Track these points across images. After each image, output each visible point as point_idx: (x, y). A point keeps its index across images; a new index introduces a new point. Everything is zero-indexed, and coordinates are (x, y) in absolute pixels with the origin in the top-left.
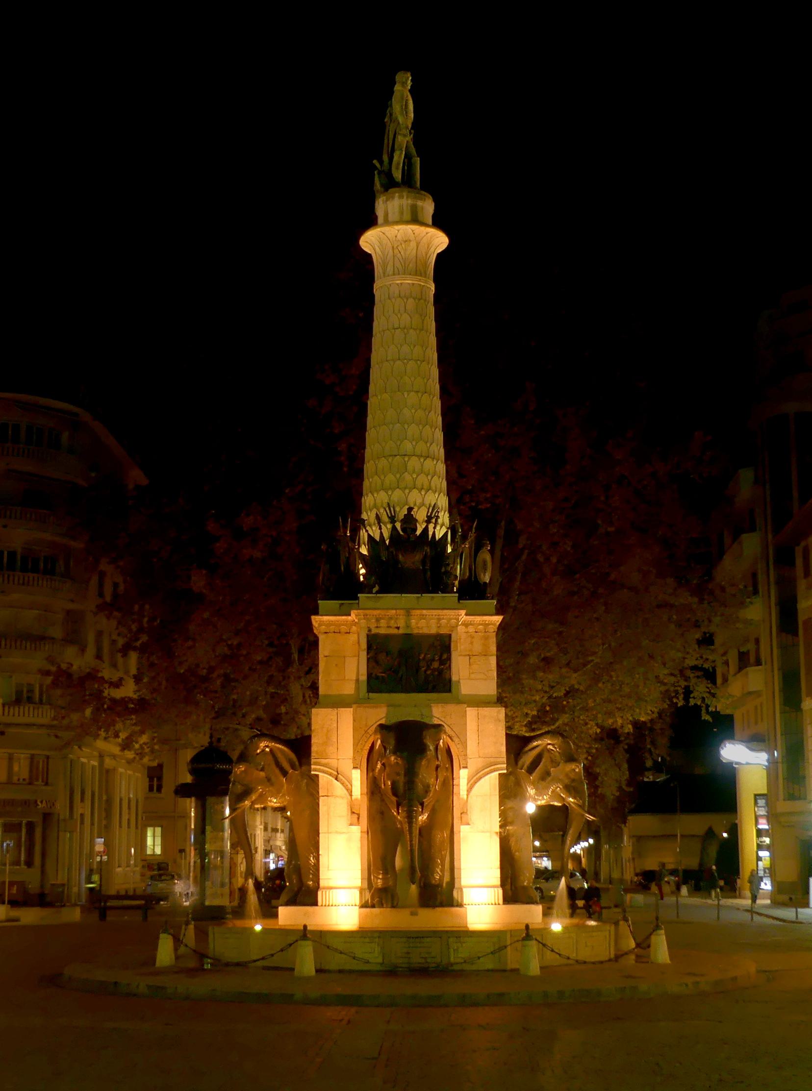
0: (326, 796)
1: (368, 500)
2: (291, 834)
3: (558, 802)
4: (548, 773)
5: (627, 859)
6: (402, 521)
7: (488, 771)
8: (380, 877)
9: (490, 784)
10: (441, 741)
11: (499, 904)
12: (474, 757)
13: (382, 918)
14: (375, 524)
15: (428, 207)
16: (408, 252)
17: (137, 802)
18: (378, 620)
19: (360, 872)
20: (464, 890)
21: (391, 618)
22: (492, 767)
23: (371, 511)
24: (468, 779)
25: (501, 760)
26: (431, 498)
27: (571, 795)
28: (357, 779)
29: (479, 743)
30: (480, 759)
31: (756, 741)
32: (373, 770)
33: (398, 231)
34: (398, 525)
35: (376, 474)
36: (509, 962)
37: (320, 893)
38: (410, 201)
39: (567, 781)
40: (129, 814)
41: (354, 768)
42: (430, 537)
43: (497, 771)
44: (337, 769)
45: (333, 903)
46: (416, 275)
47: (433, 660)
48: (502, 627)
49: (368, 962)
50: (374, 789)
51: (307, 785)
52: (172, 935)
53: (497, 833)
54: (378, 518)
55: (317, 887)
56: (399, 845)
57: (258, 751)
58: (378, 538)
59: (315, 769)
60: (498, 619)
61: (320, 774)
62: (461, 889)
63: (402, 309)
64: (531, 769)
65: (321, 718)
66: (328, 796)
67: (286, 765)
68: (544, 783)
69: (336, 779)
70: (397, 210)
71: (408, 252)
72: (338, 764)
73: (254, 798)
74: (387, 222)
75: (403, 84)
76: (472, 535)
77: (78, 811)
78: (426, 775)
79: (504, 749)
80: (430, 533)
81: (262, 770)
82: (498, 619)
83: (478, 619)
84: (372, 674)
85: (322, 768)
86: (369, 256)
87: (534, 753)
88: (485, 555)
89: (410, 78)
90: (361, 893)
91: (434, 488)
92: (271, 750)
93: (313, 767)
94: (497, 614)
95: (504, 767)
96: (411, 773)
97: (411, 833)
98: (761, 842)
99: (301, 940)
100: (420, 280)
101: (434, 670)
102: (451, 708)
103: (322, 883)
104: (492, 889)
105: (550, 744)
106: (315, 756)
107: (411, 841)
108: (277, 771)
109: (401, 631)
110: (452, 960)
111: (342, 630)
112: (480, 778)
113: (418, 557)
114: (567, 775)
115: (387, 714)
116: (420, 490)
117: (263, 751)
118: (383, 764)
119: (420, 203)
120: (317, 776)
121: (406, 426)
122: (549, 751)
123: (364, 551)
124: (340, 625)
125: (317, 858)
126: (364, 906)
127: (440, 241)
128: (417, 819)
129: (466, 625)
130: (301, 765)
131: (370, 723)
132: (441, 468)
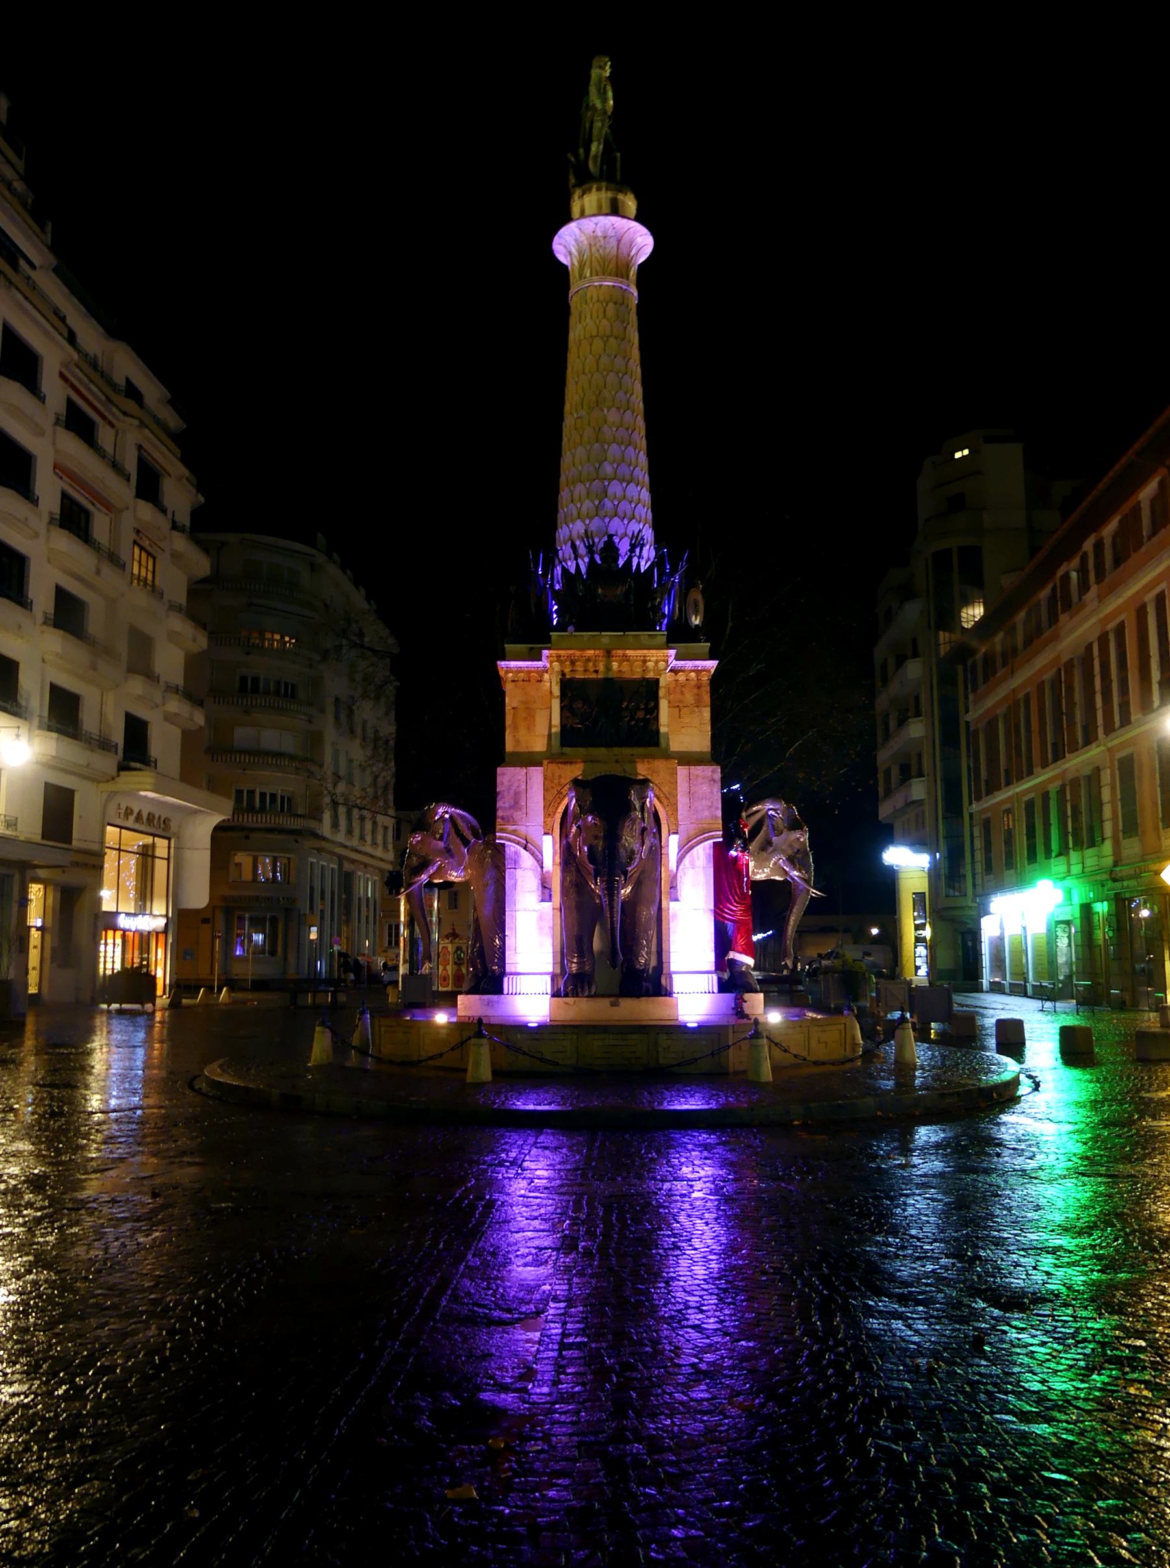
1: (562, 533)
4: (768, 843)
8: (575, 960)
9: (702, 854)
10: (648, 800)
13: (580, 1009)
14: (570, 559)
15: (630, 203)
16: (608, 251)
17: (375, 901)
18: (573, 663)
19: (551, 956)
20: (674, 976)
21: (588, 660)
23: (566, 544)
25: (716, 826)
26: (634, 527)
27: (795, 868)
28: (549, 846)
31: (919, 843)
32: (567, 836)
33: (596, 224)
35: (572, 502)
36: (731, 1065)
37: (506, 979)
38: (610, 194)
39: (790, 852)
40: (368, 911)
41: (546, 834)
42: (634, 568)
43: (708, 839)
46: (617, 276)
47: (638, 708)
48: (716, 680)
49: (557, 1064)
50: (567, 857)
51: (492, 857)
52: (329, 1028)
55: (503, 973)
56: (666, 1106)
58: (573, 571)
59: (501, 837)
60: (712, 664)
61: (507, 843)
62: (670, 976)
63: (601, 315)
65: (507, 777)
67: (467, 834)
68: (765, 854)
69: (525, 848)
70: (595, 204)
71: (608, 251)
73: (431, 872)
74: (583, 215)
75: (602, 70)
76: (682, 567)
77: (318, 906)
78: (629, 839)
79: (719, 813)
81: (441, 839)
82: (712, 664)
83: (689, 664)
84: (566, 725)
87: (753, 820)
88: (696, 595)
89: (609, 63)
90: (552, 980)
91: (638, 517)
92: (451, 817)
94: (711, 658)
96: (612, 837)
97: (612, 907)
99: (475, 1037)
100: (621, 282)
101: (639, 720)
102: (660, 764)
103: (508, 969)
104: (706, 975)
107: (612, 917)
108: (458, 841)
109: (600, 676)
110: (661, 1061)
112: (692, 848)
113: (620, 591)
114: (791, 846)
115: (583, 771)
116: (619, 444)
117: (442, 817)
118: (579, 827)
119: (620, 197)
120: (503, 845)
121: (606, 447)
124: (529, 672)
125: (503, 940)
126: (555, 994)
128: (619, 892)
129: (674, 671)
130: (485, 834)
131: (563, 781)
132: (646, 495)
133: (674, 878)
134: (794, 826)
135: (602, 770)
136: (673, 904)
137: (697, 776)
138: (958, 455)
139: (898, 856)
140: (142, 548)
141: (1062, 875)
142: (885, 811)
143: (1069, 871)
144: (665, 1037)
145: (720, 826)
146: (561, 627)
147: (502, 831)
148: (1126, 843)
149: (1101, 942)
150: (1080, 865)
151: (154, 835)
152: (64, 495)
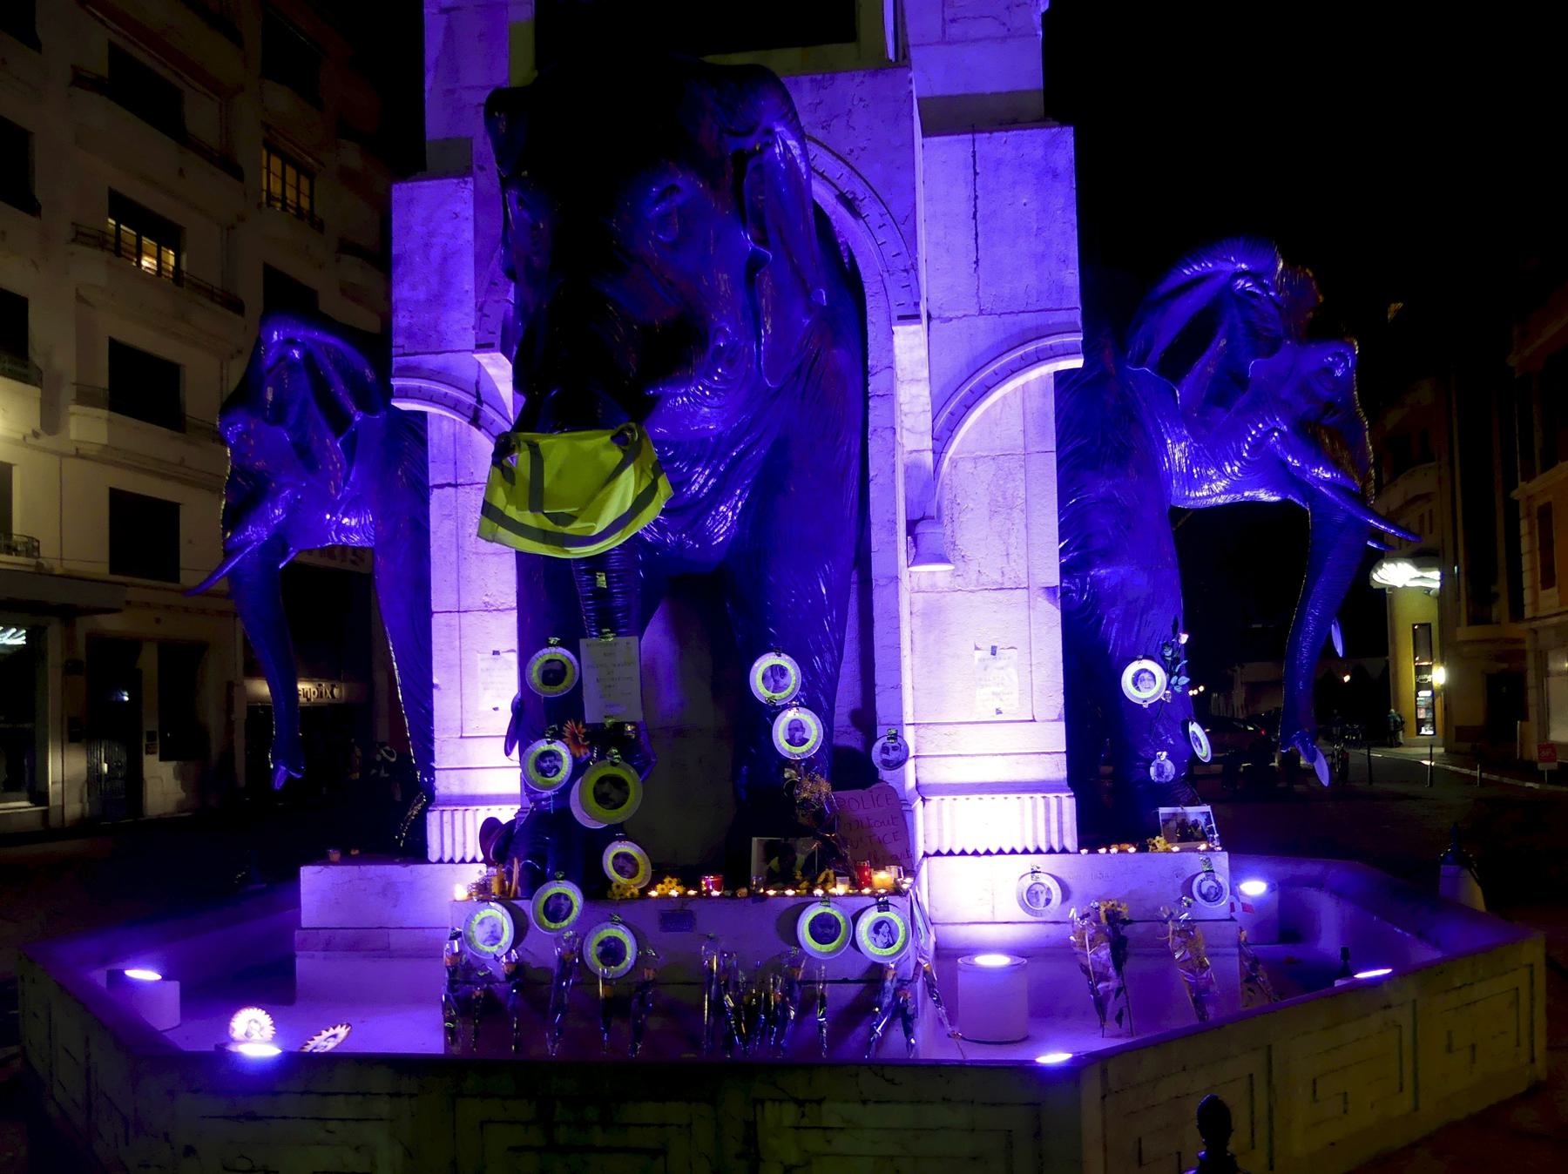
0: (449, 485)
3: (1272, 488)
5: (1240, 707)
7: (1013, 361)
11: (1064, 851)
12: (960, 314)
22: (1031, 348)
24: (934, 398)
29: (976, 262)
30: (981, 321)
37: (433, 818)
44: (477, 383)
45: (465, 853)
53: (1050, 591)
64: (1175, 364)
66: (456, 486)
85: (424, 384)
92: (307, 355)
95: (1074, 344)
98: (1421, 680)
105: (1242, 274)
106: (403, 347)
133: (927, 485)
137: (999, 163)
139: (1395, 574)
140: (287, 160)
144: (789, 1113)
145: (1077, 316)
147: (410, 371)
148: (1542, 593)
152: (112, 46)
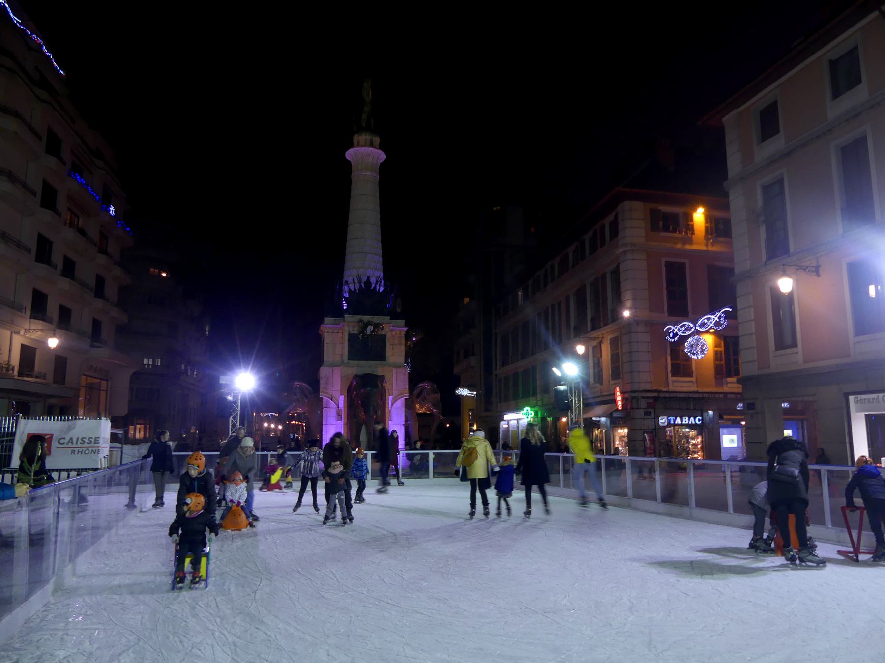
2: (733, 396)
6: (365, 283)
9: (400, 403)
15: (377, 140)
28: (342, 400)
34: (363, 285)
41: (341, 395)
54: (353, 280)
57: (294, 387)
59: (322, 395)
64: (418, 396)
65: (324, 371)
69: (331, 400)
72: (638, 419)
74: (359, 145)
80: (377, 289)
82: (406, 329)
86: (350, 162)
92: (300, 386)
93: (320, 394)
94: (406, 326)
111: (336, 332)
112: (396, 401)
119: (374, 138)
120: (322, 398)
122: (426, 388)
123: (347, 295)
127: (383, 156)
134: (434, 392)
135: (367, 371)
136: (390, 422)
138: (495, 209)
141: (533, 405)
142: (456, 370)
143: (537, 403)
146: (347, 311)
149: (549, 435)
150: (541, 401)
151: (101, 379)
